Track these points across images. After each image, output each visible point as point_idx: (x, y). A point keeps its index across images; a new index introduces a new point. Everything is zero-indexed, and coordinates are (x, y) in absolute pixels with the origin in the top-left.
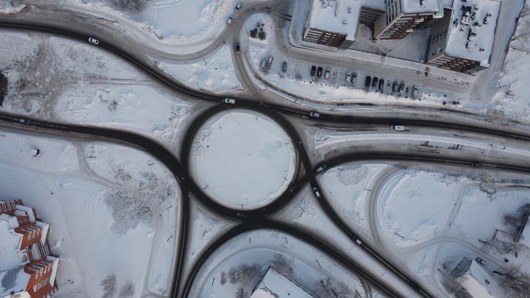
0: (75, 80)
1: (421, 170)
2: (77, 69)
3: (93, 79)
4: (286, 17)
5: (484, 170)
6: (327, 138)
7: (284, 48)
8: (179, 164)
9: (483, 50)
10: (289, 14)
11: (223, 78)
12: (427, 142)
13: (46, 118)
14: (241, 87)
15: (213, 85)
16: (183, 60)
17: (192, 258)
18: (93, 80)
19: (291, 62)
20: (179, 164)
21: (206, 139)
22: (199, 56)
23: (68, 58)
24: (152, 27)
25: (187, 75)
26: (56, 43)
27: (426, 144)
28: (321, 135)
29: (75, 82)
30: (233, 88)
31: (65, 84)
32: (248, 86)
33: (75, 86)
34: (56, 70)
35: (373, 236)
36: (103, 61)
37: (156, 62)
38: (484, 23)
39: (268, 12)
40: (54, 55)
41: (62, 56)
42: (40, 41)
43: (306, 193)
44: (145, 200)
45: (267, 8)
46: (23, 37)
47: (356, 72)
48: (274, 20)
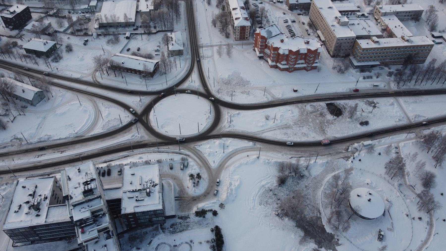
0: (295, 124)
1: (65, 138)
2: (298, 129)
3: (287, 127)
4: (179, 199)
5: (18, 149)
6: (132, 137)
7: (175, 178)
8: (218, 104)
9: (23, 187)
10: (178, 202)
11: (210, 148)
12: (61, 153)
13: (300, 105)
14: (196, 147)
15: (214, 143)
16: (239, 151)
17: (196, 69)
18: (286, 126)
19: (167, 171)
20: (218, 104)
21: (207, 116)
22: (230, 156)
23: (306, 133)
24: (267, 161)
25: (234, 144)
26: (318, 138)
27: (62, 152)
28: (137, 138)
29: (295, 123)
30: (201, 145)
31: (300, 120)
32: (192, 149)
33: (294, 121)
34: (309, 126)
35: (95, 102)
36: (286, 136)
37: (255, 145)
38: (20, 206)
39: (193, 197)
40: (315, 132)
41: (311, 133)
42: (327, 136)
43: (139, 110)
44: (229, 87)
45: (195, 200)
46: (339, 135)
47: (118, 176)
48: (187, 194)
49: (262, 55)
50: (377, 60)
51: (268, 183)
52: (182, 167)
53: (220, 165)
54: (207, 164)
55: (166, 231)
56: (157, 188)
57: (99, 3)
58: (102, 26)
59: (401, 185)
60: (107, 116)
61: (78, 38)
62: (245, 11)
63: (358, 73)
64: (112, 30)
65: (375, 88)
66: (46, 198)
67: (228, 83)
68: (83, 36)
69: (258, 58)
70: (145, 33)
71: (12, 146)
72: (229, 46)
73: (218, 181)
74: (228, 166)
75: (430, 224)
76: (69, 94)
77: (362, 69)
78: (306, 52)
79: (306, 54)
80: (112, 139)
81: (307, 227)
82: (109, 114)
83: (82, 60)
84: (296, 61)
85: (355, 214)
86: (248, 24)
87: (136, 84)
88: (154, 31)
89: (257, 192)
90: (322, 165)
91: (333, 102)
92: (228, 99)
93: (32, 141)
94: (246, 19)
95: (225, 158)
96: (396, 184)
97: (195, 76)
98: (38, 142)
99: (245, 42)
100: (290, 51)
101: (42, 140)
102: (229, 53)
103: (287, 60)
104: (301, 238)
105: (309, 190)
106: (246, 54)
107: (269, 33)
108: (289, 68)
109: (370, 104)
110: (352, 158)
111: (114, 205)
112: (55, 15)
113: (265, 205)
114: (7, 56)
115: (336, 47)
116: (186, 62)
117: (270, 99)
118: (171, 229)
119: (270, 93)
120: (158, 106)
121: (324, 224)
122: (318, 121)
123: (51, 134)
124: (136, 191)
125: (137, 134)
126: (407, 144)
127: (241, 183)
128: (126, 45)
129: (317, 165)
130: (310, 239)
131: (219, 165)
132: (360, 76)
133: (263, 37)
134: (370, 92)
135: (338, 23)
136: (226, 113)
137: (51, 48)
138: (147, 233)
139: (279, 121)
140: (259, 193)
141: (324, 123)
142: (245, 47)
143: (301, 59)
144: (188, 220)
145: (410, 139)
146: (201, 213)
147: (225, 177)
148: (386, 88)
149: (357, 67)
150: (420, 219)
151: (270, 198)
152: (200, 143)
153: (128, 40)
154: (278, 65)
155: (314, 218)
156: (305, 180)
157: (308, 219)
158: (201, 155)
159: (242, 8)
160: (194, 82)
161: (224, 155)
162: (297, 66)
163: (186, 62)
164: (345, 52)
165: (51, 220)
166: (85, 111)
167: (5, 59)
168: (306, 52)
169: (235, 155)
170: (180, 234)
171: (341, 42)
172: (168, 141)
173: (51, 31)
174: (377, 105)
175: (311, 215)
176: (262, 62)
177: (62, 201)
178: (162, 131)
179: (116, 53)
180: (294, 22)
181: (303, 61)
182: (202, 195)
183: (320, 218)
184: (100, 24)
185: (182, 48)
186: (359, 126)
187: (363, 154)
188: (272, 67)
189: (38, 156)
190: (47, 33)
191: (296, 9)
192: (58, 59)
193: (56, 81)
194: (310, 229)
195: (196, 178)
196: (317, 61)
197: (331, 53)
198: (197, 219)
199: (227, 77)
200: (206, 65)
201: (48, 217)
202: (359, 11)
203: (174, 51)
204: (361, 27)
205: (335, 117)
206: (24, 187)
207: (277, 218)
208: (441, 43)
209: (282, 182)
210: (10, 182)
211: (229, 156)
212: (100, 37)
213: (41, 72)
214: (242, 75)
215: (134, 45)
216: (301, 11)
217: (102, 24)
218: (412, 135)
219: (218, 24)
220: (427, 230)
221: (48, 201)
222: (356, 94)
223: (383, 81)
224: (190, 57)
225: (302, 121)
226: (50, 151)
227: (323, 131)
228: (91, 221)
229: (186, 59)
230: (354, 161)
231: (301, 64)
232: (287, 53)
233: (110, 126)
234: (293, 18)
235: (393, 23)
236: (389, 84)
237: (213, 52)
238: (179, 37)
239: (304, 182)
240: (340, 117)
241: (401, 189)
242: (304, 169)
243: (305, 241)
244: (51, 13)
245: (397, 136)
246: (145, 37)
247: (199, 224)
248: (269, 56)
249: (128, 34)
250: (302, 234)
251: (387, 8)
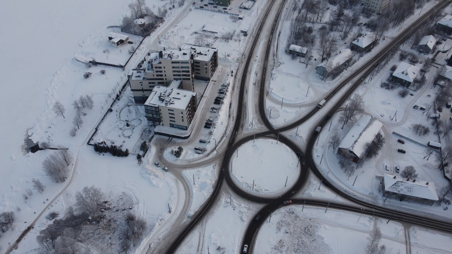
8: (269, 206)
11: (206, 174)
35: (310, 106)
39: (164, 149)
44: (299, 230)
45: (161, 150)
51: (138, 209)
53: (182, 177)
54: (190, 167)
80: (254, 110)
81: (77, 220)
95: (188, 184)
105: (106, 245)
113: (121, 197)
130: (67, 218)
131: (183, 176)
140: (134, 197)
146: (144, 148)
147: (169, 177)
156: (118, 248)
157: (82, 226)
169: (186, 194)
172: (233, 145)
175: (84, 231)
177: (198, 75)
182: (162, 155)
189: (256, 74)
209: (130, 219)
211: (188, 188)
239: (117, 245)
243: (69, 212)
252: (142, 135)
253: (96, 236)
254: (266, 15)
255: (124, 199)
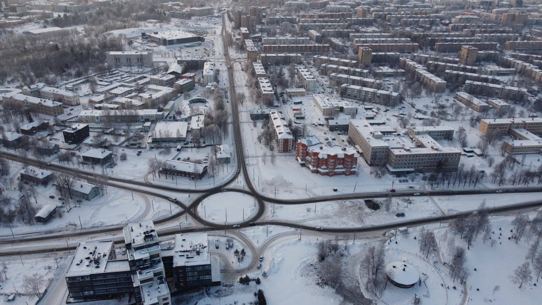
0: (335, 215)
1: (117, 225)
2: (338, 219)
3: (327, 217)
7: (220, 256)
8: (261, 200)
10: (223, 274)
11: (254, 232)
13: (340, 201)
20: (261, 200)
23: (346, 222)
26: (358, 226)
27: (114, 235)
38: (82, 260)
39: (238, 270)
46: (376, 224)
48: (232, 268)
49: (304, 162)
50: (412, 167)
51: (309, 260)
52: (227, 246)
53: (264, 246)
55: (212, 296)
56: (206, 249)
57: (152, 125)
58: (155, 141)
59: (435, 262)
60: (158, 208)
61: (132, 150)
62: (288, 128)
63: (395, 178)
64: (164, 145)
65: (411, 189)
66: (105, 255)
67: (271, 184)
68: (137, 148)
69: (300, 166)
70: (195, 147)
71: (67, 230)
72: (273, 156)
73: (261, 257)
74: (272, 246)
75: (465, 293)
76: (122, 192)
77: (398, 174)
78: (343, 157)
79: (343, 159)
82: (159, 207)
83: (135, 166)
84: (335, 165)
85: (390, 282)
86: (291, 137)
87: (185, 184)
88: (203, 145)
89: (298, 266)
90: (361, 246)
91: (371, 199)
92: (271, 196)
93: (86, 226)
94: (289, 133)
96: (431, 262)
97: (241, 179)
98: (92, 228)
99: (287, 154)
100: (329, 156)
101: (95, 226)
102: (273, 161)
103: (327, 164)
104: (340, 302)
106: (289, 162)
107: (310, 142)
108: (329, 172)
109: (406, 201)
110: (389, 241)
111: (168, 261)
112: (112, 133)
114: (66, 163)
115: (372, 156)
116: (232, 169)
117: (312, 196)
118: (216, 294)
119: (311, 192)
120: (206, 201)
121: (362, 291)
122: (356, 213)
123: (105, 221)
124: (187, 251)
125: (186, 221)
126: (439, 231)
127: (283, 259)
128: (177, 155)
129: (357, 247)
132: (397, 180)
133: (303, 145)
134: (406, 192)
135: (373, 136)
136: (269, 206)
137: (107, 156)
138: (193, 297)
139: (320, 213)
141: (362, 214)
142: (287, 157)
143: (339, 164)
144: (232, 287)
145: (444, 227)
147: (268, 255)
148: (422, 189)
149: (393, 173)
150: (455, 288)
151: (311, 271)
152: (244, 229)
153: (178, 152)
154: (319, 169)
155: (353, 287)
158: (246, 238)
159: (286, 126)
160: (240, 183)
161: (267, 238)
162: (336, 170)
163: (232, 169)
164: (381, 160)
165: (109, 271)
166: (137, 204)
167: (63, 165)
168: (343, 157)
170: (224, 298)
171: (376, 151)
173: (107, 144)
174: (413, 202)
176: (304, 169)
178: (210, 220)
179: (169, 160)
180: (334, 139)
181: (341, 166)
183: (359, 287)
184: (153, 139)
185: (229, 156)
186: (396, 217)
187: (399, 238)
188: (313, 172)
189: (92, 238)
190: (104, 146)
191: (336, 130)
192: (112, 165)
193: (110, 182)
194: (350, 295)
195: (241, 255)
196: (355, 166)
197: (369, 162)
198: (241, 286)
199: (271, 179)
200: (250, 170)
201: (107, 268)
202: (395, 132)
203: (221, 159)
204: (395, 142)
205: (373, 211)
206: (85, 248)
207: (318, 287)
208: (472, 156)
209: (322, 258)
210: (64, 257)
212: (153, 150)
213: (96, 175)
214: (285, 178)
215: (184, 155)
216: (341, 131)
217: (156, 139)
218: (446, 225)
219: (263, 139)
220: (461, 297)
221: (107, 257)
222: (393, 194)
223: (418, 184)
224: (237, 164)
225: (341, 213)
226: (103, 234)
227: (362, 221)
228: (148, 264)
229: (233, 167)
230: (390, 243)
231: (340, 169)
232: (326, 157)
233: (160, 215)
234: (333, 137)
235: (427, 140)
236: (424, 186)
237: (258, 161)
238: (226, 149)
240: (378, 211)
241: (436, 265)
242: (344, 249)
244: (108, 131)
245: (432, 224)
246: (194, 150)
247: (243, 290)
248: (310, 163)
249: (179, 147)
250: (342, 299)
251: (419, 128)
252: (225, 296)
253: (347, 275)
254: (13, 242)
255: (306, 273)
